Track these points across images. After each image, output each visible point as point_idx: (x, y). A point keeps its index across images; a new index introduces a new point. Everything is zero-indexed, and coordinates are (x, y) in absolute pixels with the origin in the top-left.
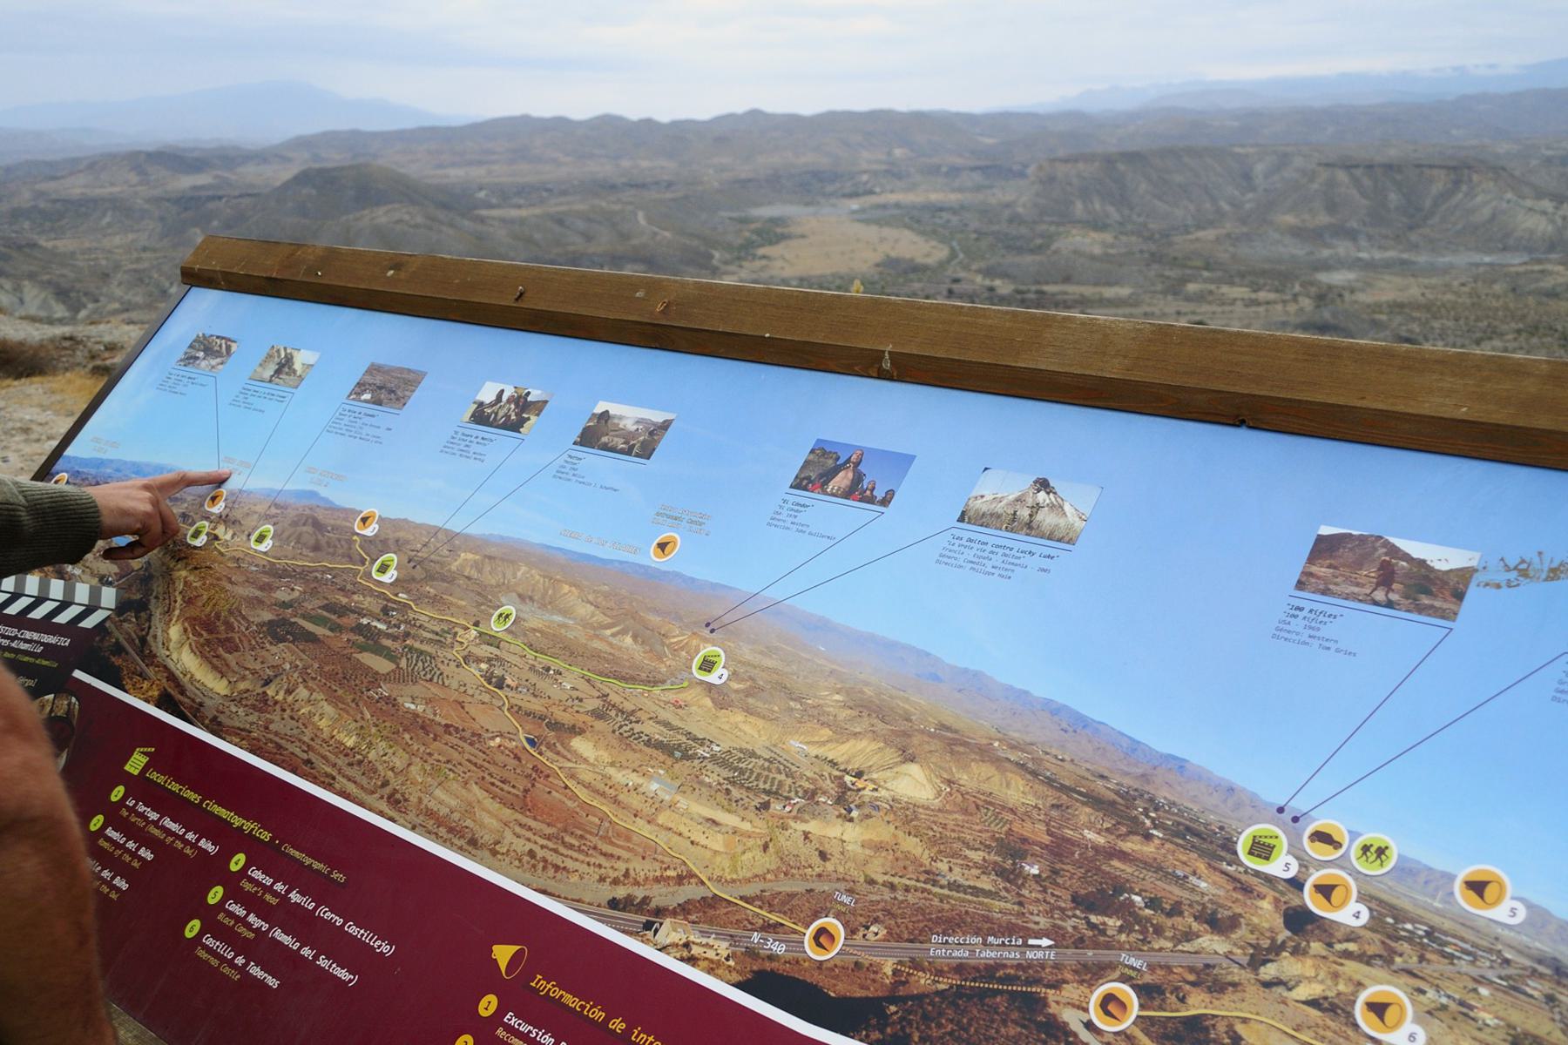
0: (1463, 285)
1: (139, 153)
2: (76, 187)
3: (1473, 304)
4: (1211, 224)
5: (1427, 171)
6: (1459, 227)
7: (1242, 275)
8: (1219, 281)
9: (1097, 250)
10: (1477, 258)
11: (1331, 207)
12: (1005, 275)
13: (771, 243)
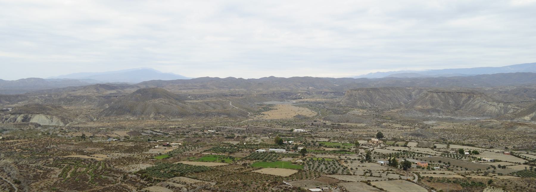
1: (98, 84)
2: (78, 93)
4: (397, 108)
7: (200, 97)
8: (394, 123)
9: (360, 114)
10: (474, 118)
11: (432, 104)
12: (329, 120)
13: (266, 111)
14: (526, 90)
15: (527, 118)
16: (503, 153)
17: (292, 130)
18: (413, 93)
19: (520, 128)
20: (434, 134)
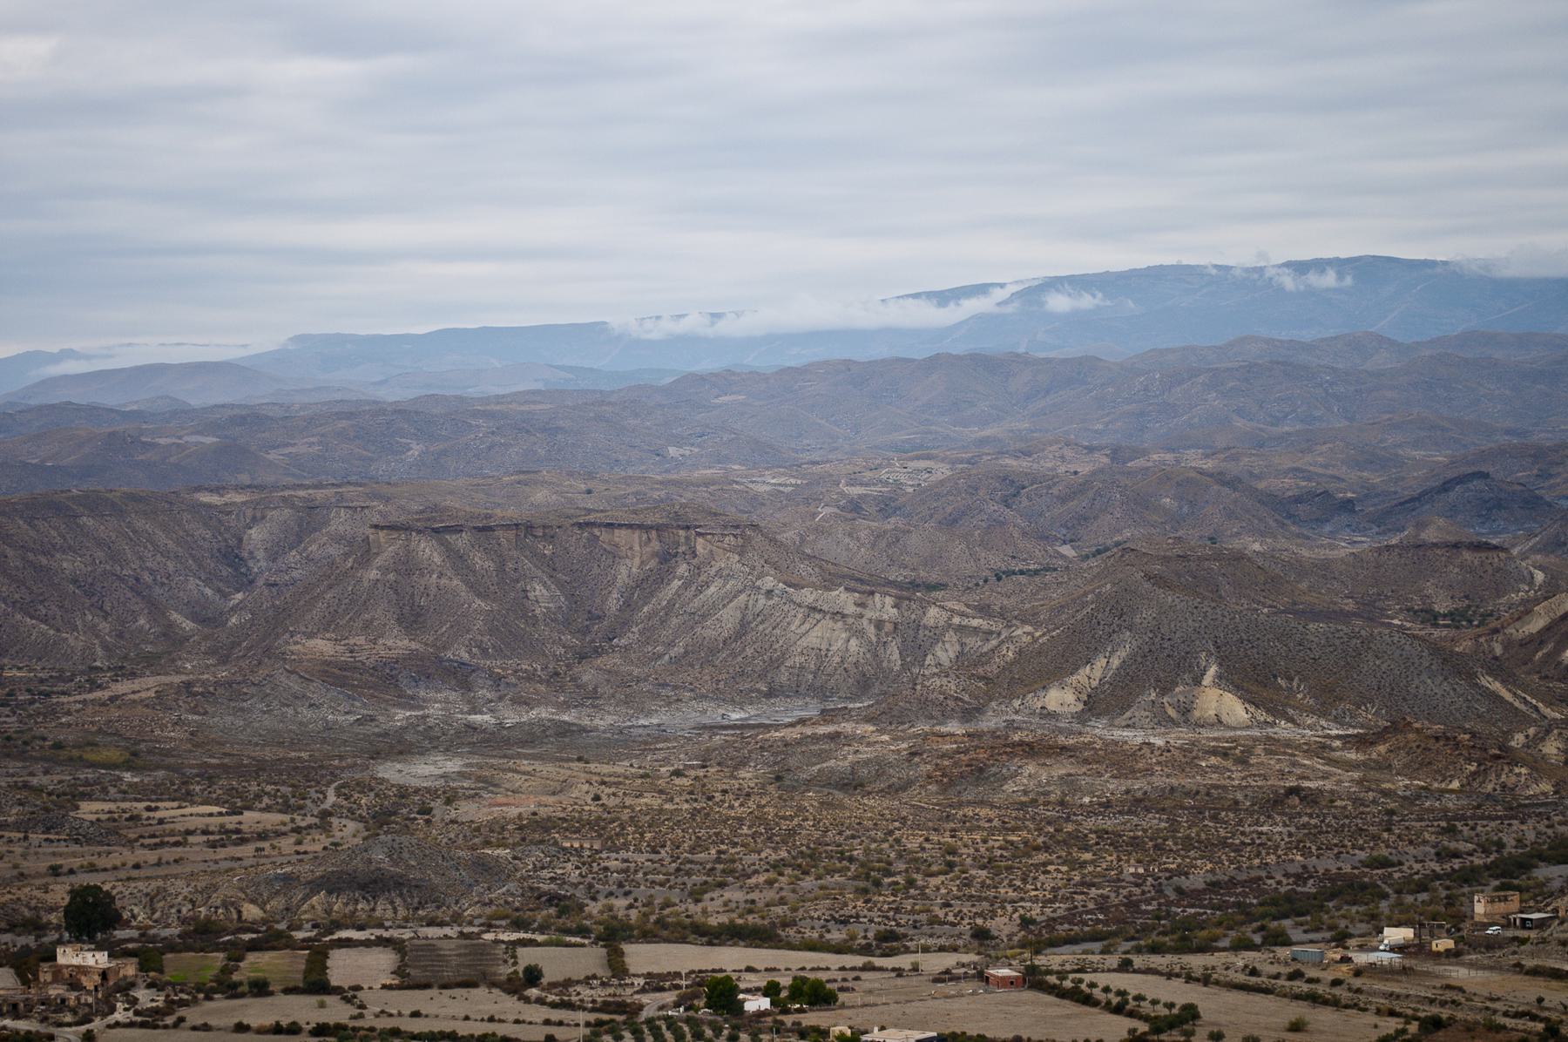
0: (677, 773)
3: (694, 813)
4: (151, 663)
5: (604, 535)
6: (678, 650)
8: (156, 793)
11: (412, 620)
14: (1012, 488)
15: (1060, 699)
16: (982, 977)
18: (256, 534)
19: (1030, 775)
20: (485, 869)
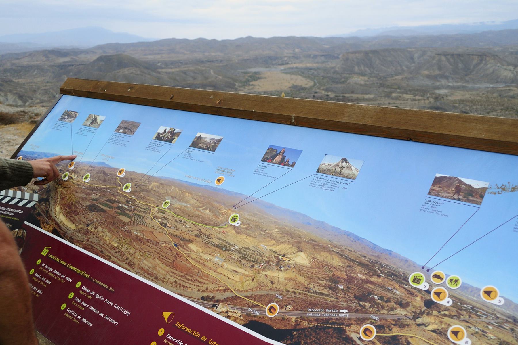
1: (46, 50)
2: (25, 62)
4: (400, 74)
9: (362, 83)
10: (488, 85)
11: (440, 68)
12: (332, 91)
13: (255, 80)
17: (370, 307)
